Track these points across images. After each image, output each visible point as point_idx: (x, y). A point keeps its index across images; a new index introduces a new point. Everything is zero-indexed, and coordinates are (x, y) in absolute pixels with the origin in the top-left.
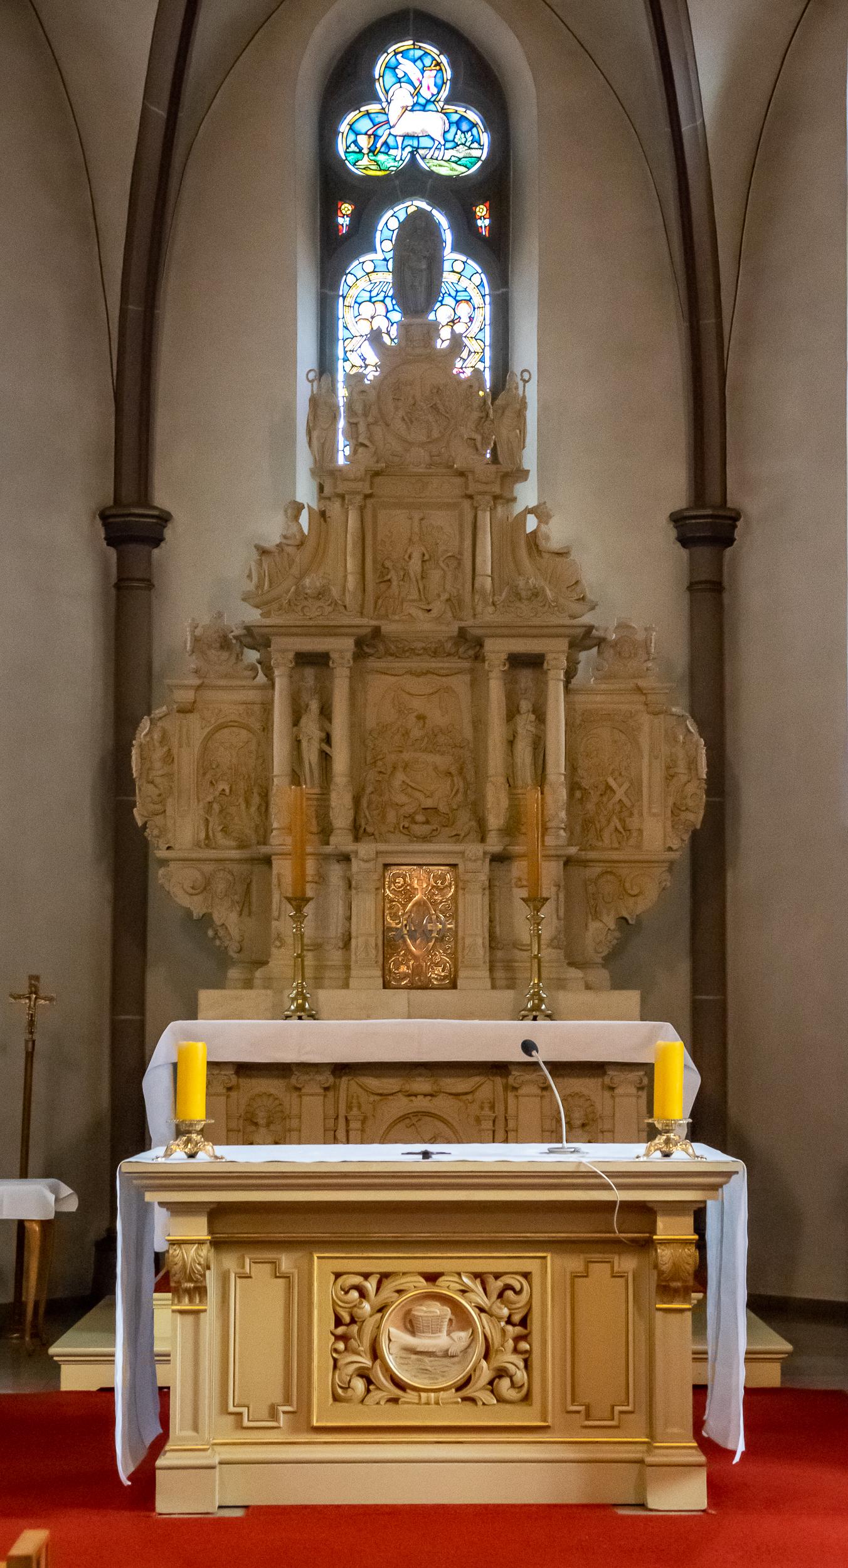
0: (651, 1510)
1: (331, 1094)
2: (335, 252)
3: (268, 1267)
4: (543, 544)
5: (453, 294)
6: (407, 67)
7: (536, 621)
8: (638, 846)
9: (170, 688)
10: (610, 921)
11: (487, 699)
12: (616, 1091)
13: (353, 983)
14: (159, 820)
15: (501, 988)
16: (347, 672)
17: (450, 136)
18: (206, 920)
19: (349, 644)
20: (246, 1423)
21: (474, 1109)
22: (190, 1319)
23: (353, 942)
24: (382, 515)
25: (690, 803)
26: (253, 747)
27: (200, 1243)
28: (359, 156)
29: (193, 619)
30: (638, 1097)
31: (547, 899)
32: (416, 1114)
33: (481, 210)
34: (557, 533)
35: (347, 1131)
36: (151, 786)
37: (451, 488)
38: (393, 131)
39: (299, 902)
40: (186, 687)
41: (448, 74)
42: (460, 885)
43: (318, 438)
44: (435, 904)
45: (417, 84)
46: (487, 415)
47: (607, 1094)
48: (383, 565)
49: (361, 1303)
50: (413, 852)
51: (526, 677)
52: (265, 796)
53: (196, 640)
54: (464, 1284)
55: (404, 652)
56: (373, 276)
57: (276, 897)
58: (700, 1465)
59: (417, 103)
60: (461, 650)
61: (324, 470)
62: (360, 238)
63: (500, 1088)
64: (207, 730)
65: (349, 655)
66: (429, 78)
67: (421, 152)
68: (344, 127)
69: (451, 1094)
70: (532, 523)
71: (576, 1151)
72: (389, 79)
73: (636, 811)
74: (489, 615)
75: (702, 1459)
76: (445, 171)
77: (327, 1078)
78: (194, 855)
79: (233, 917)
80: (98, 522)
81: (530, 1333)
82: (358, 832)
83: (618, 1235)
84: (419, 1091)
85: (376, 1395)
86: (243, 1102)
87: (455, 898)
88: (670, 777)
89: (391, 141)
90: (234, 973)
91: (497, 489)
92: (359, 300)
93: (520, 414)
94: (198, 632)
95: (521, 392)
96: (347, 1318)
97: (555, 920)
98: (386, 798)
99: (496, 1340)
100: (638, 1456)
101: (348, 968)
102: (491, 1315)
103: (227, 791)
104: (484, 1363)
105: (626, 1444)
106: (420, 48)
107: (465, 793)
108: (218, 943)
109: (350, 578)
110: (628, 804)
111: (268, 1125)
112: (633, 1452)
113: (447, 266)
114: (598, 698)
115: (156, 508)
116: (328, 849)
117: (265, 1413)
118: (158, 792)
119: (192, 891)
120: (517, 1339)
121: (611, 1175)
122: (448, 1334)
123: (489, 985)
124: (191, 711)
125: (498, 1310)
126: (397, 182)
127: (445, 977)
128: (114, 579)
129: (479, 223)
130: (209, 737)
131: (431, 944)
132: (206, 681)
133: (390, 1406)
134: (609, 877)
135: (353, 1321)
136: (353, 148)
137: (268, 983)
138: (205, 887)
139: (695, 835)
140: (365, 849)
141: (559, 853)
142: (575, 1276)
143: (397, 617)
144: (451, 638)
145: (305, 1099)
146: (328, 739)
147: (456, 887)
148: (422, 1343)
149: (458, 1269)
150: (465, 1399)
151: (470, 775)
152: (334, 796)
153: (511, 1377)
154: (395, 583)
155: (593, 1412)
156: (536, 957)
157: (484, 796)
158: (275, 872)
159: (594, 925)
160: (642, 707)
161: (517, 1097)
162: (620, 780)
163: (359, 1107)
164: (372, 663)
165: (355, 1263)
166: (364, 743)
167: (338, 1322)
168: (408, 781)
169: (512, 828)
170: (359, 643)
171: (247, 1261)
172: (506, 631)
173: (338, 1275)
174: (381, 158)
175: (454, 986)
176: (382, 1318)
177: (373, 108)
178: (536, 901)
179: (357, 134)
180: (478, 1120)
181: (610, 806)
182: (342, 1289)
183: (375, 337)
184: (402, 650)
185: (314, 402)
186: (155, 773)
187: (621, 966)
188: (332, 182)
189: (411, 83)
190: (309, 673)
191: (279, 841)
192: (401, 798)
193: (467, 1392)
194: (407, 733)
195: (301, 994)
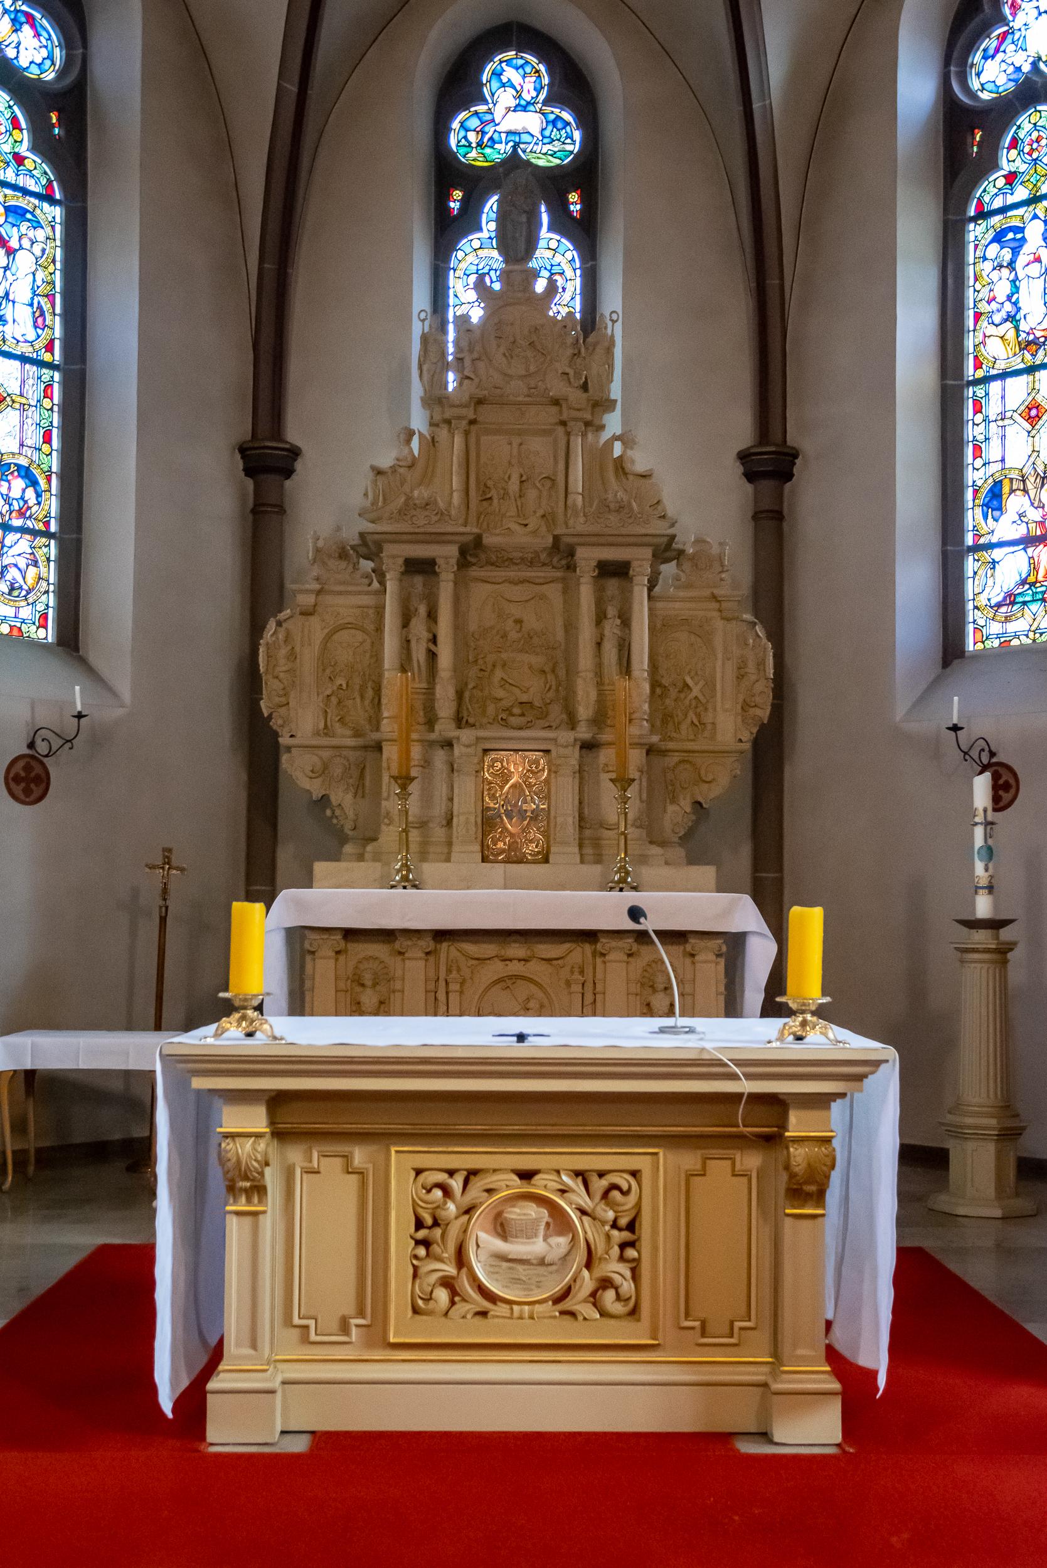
0: (777, 1444)
1: (432, 959)
2: (447, 231)
3: (338, 1160)
4: (628, 466)
5: (549, 267)
6: (510, 74)
7: (624, 531)
8: (713, 737)
9: (294, 593)
10: (686, 805)
11: (578, 605)
12: (697, 958)
13: (454, 856)
14: (283, 711)
15: (589, 863)
16: (451, 576)
17: (547, 133)
18: (324, 800)
19: (453, 551)
20: (313, 1337)
21: (565, 973)
22: (247, 1220)
23: (455, 820)
24: (484, 439)
25: (758, 699)
26: (367, 646)
27: (258, 1136)
28: (469, 149)
29: (315, 532)
30: (717, 963)
31: (634, 780)
32: (510, 977)
33: (573, 197)
34: (640, 461)
35: (447, 993)
36: (276, 681)
37: (547, 416)
38: (498, 128)
39: (404, 780)
40: (307, 591)
41: (546, 80)
42: (554, 770)
43: (429, 370)
44: (530, 786)
45: (519, 88)
46: (579, 352)
47: (688, 961)
48: (485, 485)
49: (445, 1203)
50: (511, 739)
51: (612, 585)
52: (378, 691)
53: (318, 551)
54: (563, 1183)
55: (504, 562)
56: (480, 252)
57: (386, 778)
58: (836, 1394)
59: (518, 105)
60: (555, 560)
61: (435, 399)
62: (469, 221)
63: (589, 955)
64: (326, 631)
65: (454, 561)
66: (529, 85)
67: (522, 146)
68: (455, 125)
69: (543, 959)
70: (618, 449)
71: (691, 1031)
72: (495, 84)
73: (710, 706)
74: (579, 525)
75: (836, 1386)
76: (541, 163)
77: (428, 943)
78: (314, 742)
79: (349, 797)
80: (238, 456)
81: (639, 1239)
82: (460, 721)
83: (742, 1129)
84: (516, 956)
85: (461, 1308)
86: (352, 964)
87: (547, 781)
88: (740, 677)
89: (496, 136)
90: (348, 849)
91: (588, 417)
92: (468, 272)
93: (609, 351)
94: (320, 544)
95: (609, 331)
96: (429, 1221)
97: (638, 801)
98: (486, 692)
99: (600, 1247)
100: (761, 1378)
101: (450, 844)
102: (594, 1219)
103: (344, 686)
104: (585, 1273)
105: (749, 1363)
106: (522, 58)
107: (557, 690)
108: (335, 821)
109: (455, 495)
110: (704, 701)
111: (375, 985)
112: (754, 1374)
113: (542, 244)
114: (677, 605)
115: (287, 442)
116: (433, 736)
117: (335, 1326)
118: (282, 686)
119: (311, 774)
120: (623, 1246)
121: (738, 1063)
122: (545, 1240)
123: (578, 860)
124: (311, 614)
125: (603, 1214)
126: (501, 170)
127: (539, 853)
128: (250, 503)
129: (572, 207)
130: (328, 638)
131: (526, 822)
132: (326, 587)
133: (478, 1320)
134: (688, 766)
135: (436, 1223)
136: (463, 142)
137: (377, 857)
138: (323, 771)
139: (762, 727)
140: (466, 735)
141: (642, 741)
142: (689, 1176)
143: (498, 531)
144: (545, 549)
145: (407, 962)
146: (434, 640)
147: (549, 771)
148: (515, 1250)
149: (555, 1166)
150: (562, 1313)
151: (562, 673)
152: (438, 688)
153: (616, 1289)
154: (495, 501)
155: (709, 1329)
156: (623, 833)
157: (575, 692)
158: (384, 756)
159: (671, 808)
160: (716, 614)
161: (604, 962)
162: (696, 678)
163: (459, 970)
164: (474, 572)
165: (437, 1158)
166: (467, 645)
167: (419, 1224)
168: (506, 678)
169: (599, 719)
170: (463, 552)
171: (315, 1155)
172: (594, 539)
173: (419, 1172)
174: (488, 151)
175: (546, 860)
176: (469, 1220)
177: (481, 108)
178: (623, 782)
179: (467, 130)
180: (568, 984)
181: (687, 702)
182: (423, 1187)
183: (480, 286)
184: (502, 560)
185: (425, 339)
186: (278, 669)
187: (694, 846)
188: (446, 171)
189: (514, 87)
190: (418, 580)
191: (388, 728)
192: (500, 693)
193: (566, 1305)
194: (504, 636)
195: (405, 866)
